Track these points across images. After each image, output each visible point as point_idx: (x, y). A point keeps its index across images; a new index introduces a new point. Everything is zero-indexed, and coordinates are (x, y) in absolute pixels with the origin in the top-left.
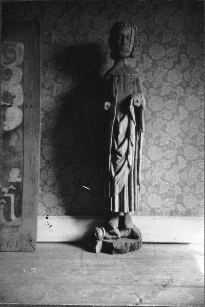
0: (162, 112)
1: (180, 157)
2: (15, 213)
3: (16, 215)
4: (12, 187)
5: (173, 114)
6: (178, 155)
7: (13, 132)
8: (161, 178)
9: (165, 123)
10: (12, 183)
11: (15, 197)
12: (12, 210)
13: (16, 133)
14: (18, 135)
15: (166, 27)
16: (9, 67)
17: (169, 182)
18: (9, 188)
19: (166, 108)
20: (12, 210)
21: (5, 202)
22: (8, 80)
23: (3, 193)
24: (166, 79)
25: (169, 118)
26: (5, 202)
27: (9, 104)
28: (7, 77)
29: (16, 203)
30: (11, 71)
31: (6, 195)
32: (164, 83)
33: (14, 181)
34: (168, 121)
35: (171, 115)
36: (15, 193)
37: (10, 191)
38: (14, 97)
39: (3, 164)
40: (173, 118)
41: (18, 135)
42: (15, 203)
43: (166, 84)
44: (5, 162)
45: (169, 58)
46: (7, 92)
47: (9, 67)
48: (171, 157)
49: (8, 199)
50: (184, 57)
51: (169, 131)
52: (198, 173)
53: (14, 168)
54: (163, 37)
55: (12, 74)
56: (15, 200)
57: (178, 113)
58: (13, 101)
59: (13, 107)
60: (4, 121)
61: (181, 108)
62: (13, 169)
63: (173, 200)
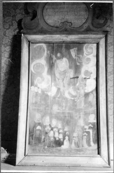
0: (4, 53)
1: (14, 21)
2: (93, 141)
3: (94, 143)
4: (91, 125)
5: (10, 25)
6: (13, 20)
7: (91, 93)
8: (4, 34)
9: (5, 31)
10: (91, 123)
11: (93, 131)
12: (91, 140)
13: (92, 93)
14: (93, 94)
15: (5, 35)
16: (88, 57)
17: (8, 36)
18: (89, 126)
19: (5, 22)
20: (91, 140)
21: (87, 135)
22: (88, 63)
23: (85, 129)
24: (5, 35)
25: (8, 28)
26: (87, 135)
27: (88, 77)
28: (87, 62)
29: (94, 135)
30: (90, 59)
31: (87, 130)
32: (5, 36)
33: (91, 122)
34: (7, 29)
35: (8, 25)
36: (93, 129)
37: (90, 128)
38: (91, 73)
39: (85, 112)
40: (9, 28)
41: (93, 94)
42: (93, 136)
43: (6, 37)
44: (86, 111)
45: (6, 23)
46: (87, 71)
47: (88, 57)
48: (9, 22)
49: (88, 133)
50: (14, 22)
51: (8, 35)
52: (5, 60)
53: (92, 114)
54: (3, 40)
55: (90, 61)
56: (93, 134)
57: (12, 25)
58: (90, 75)
59: (90, 79)
60: (85, 86)
61: (13, 22)
62: (91, 115)
63: (10, 18)
